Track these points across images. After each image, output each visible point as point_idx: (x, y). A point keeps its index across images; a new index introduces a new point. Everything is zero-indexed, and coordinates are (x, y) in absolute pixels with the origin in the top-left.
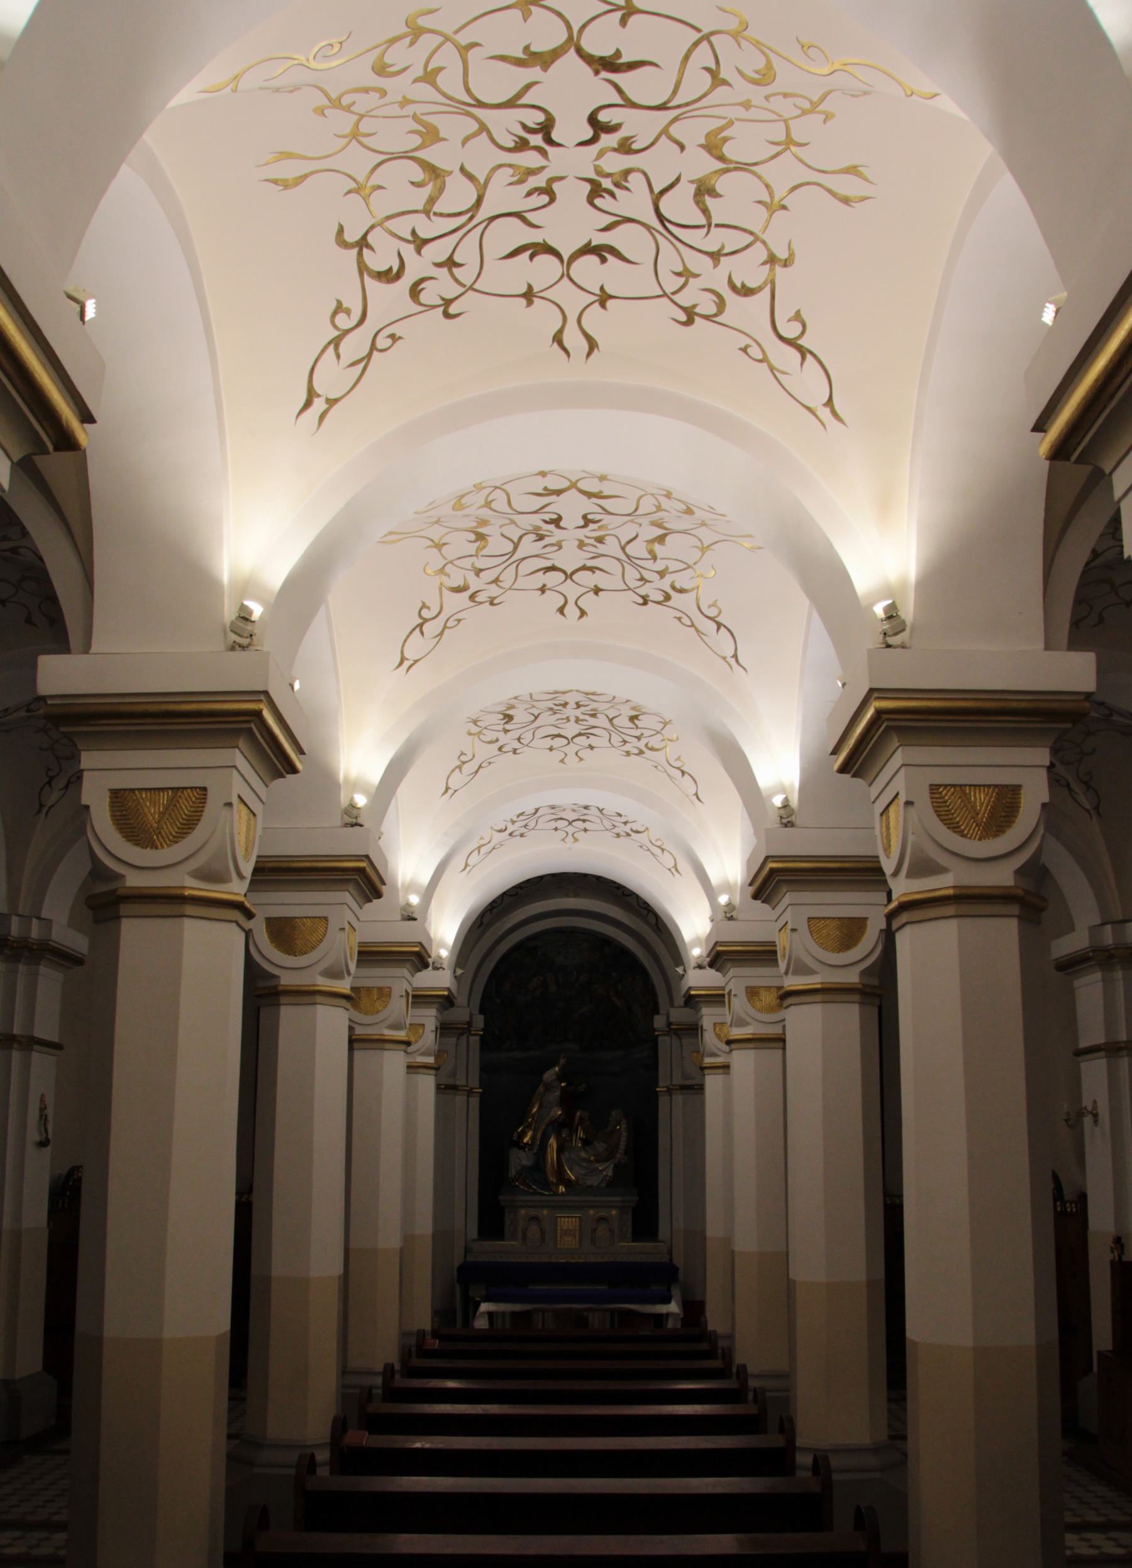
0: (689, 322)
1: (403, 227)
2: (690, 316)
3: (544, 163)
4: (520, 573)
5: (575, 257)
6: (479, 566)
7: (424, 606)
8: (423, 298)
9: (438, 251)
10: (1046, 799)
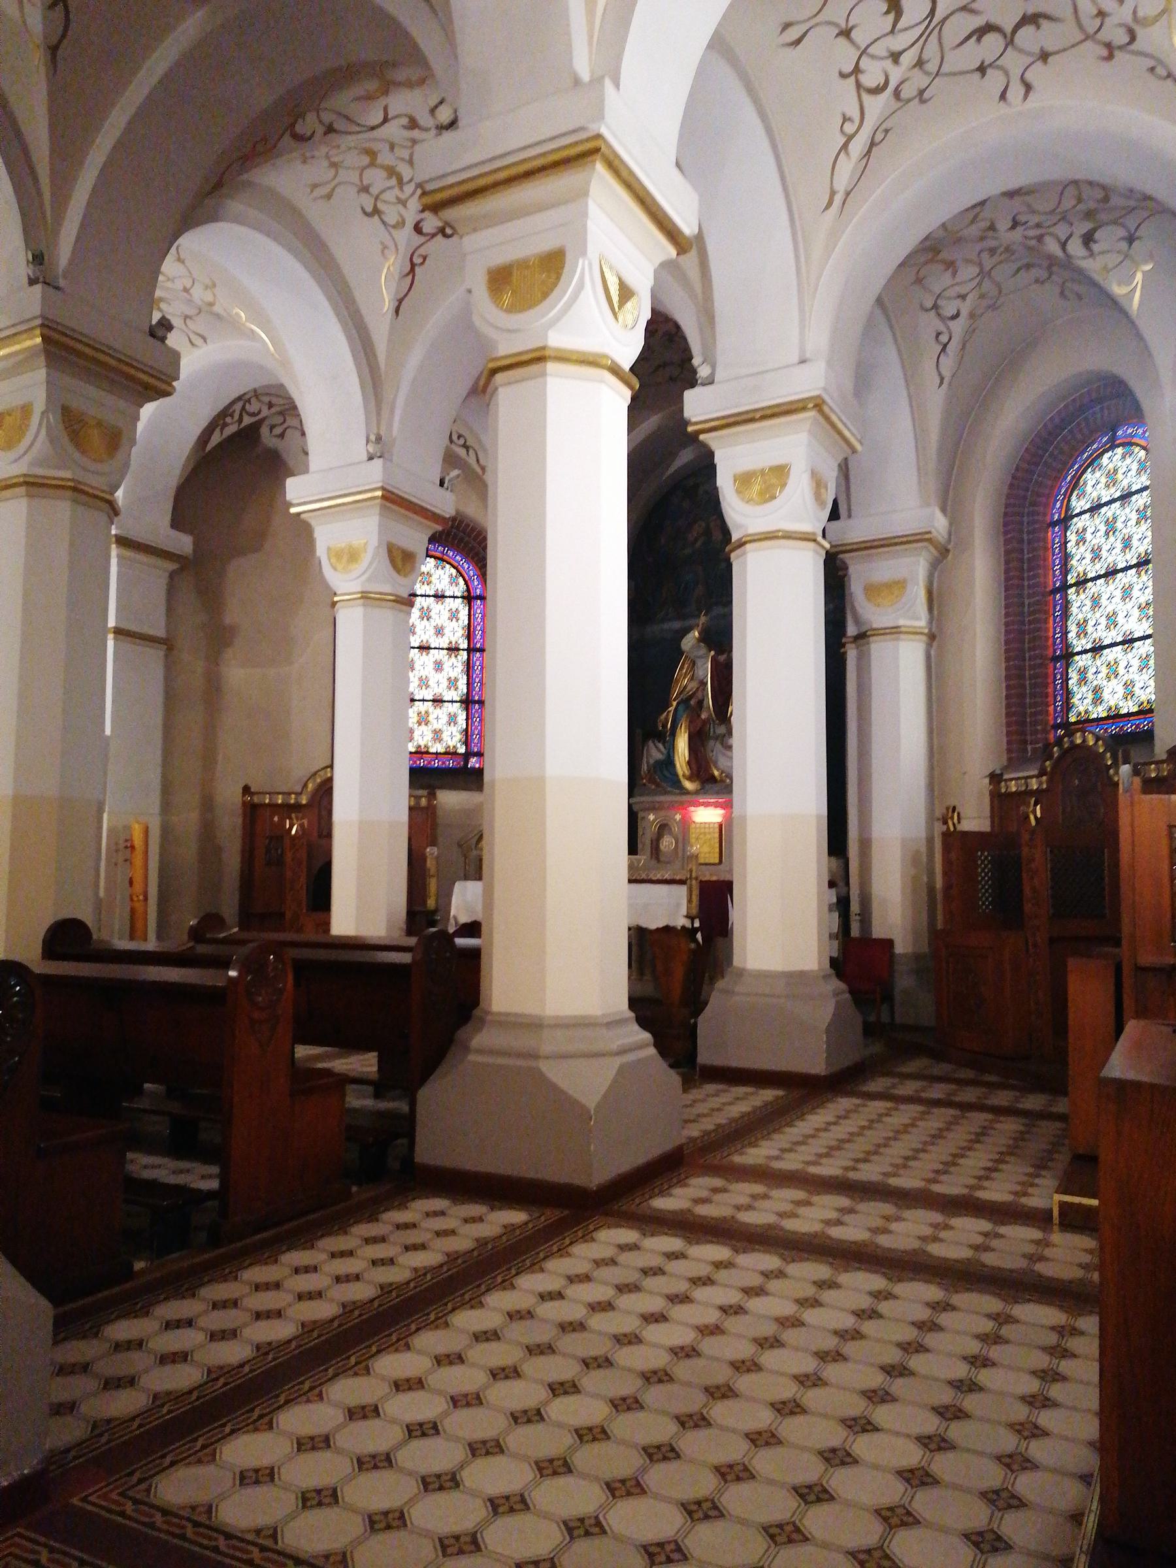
0: (1110, 57)
1: (879, 49)
2: (1111, 51)
3: (1025, 233)
4: (945, 41)
5: (1014, 31)
6: (897, 47)
7: (846, 119)
8: (903, 95)
9: (908, 59)
10: (835, 955)
